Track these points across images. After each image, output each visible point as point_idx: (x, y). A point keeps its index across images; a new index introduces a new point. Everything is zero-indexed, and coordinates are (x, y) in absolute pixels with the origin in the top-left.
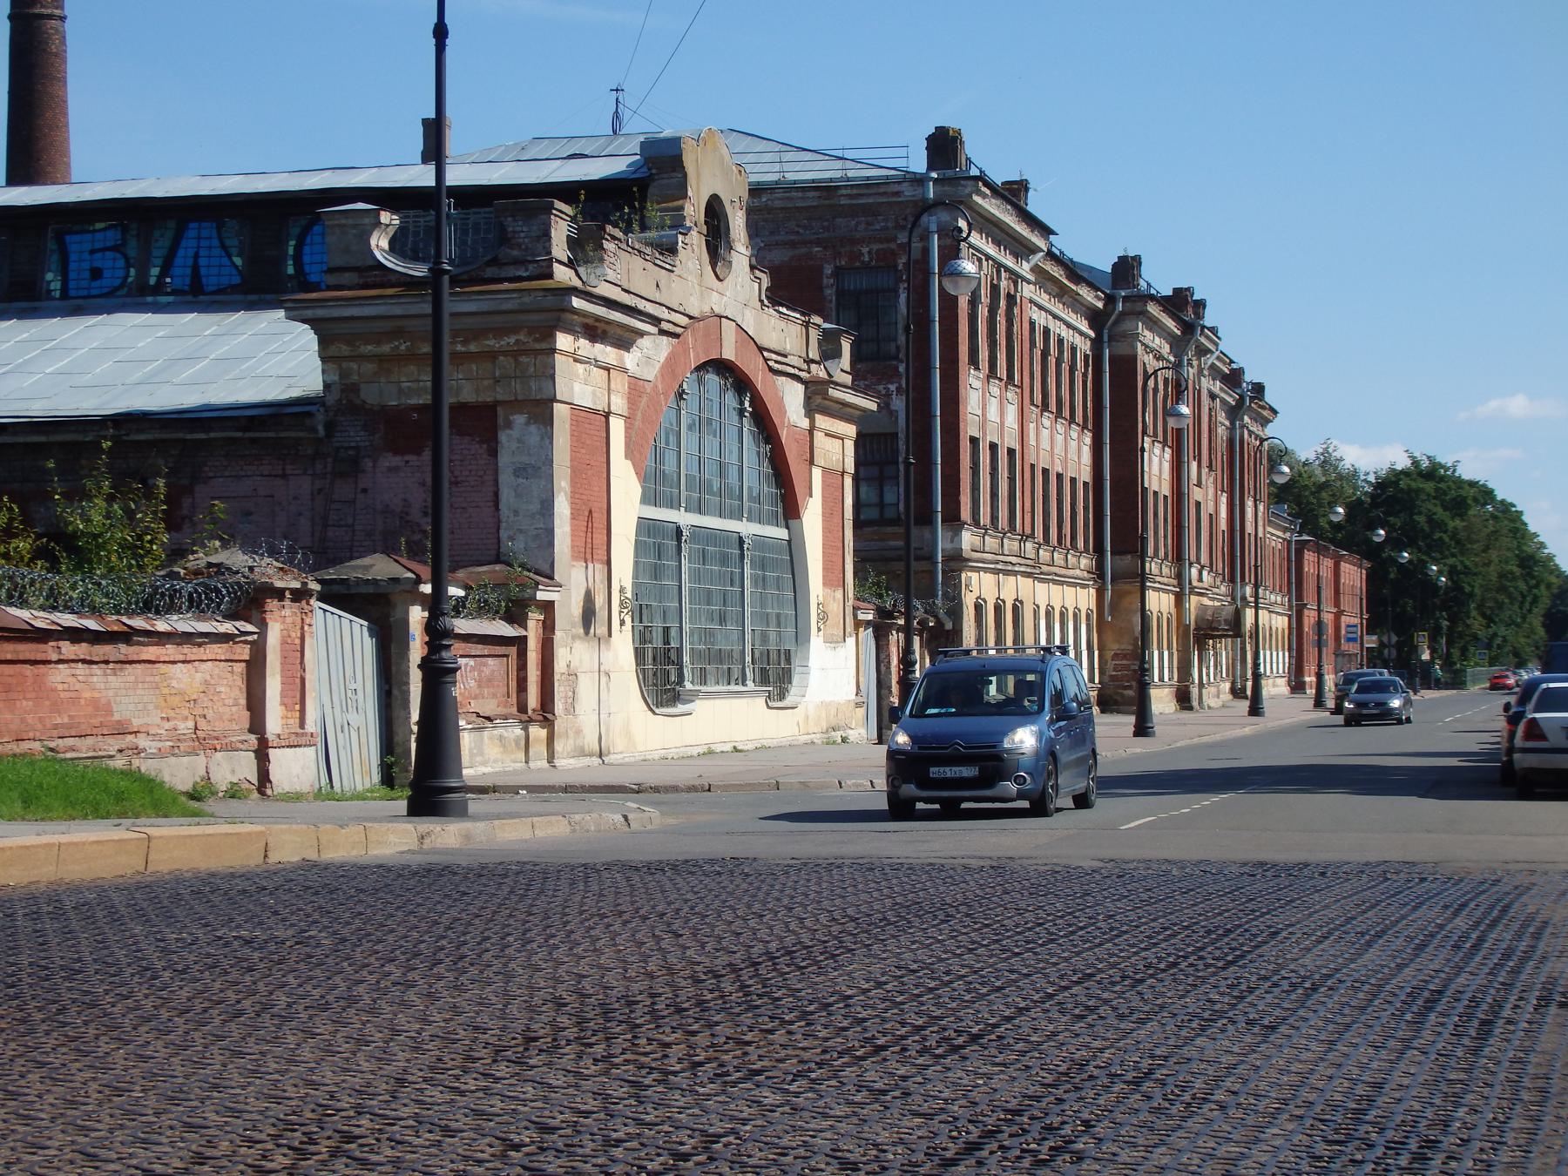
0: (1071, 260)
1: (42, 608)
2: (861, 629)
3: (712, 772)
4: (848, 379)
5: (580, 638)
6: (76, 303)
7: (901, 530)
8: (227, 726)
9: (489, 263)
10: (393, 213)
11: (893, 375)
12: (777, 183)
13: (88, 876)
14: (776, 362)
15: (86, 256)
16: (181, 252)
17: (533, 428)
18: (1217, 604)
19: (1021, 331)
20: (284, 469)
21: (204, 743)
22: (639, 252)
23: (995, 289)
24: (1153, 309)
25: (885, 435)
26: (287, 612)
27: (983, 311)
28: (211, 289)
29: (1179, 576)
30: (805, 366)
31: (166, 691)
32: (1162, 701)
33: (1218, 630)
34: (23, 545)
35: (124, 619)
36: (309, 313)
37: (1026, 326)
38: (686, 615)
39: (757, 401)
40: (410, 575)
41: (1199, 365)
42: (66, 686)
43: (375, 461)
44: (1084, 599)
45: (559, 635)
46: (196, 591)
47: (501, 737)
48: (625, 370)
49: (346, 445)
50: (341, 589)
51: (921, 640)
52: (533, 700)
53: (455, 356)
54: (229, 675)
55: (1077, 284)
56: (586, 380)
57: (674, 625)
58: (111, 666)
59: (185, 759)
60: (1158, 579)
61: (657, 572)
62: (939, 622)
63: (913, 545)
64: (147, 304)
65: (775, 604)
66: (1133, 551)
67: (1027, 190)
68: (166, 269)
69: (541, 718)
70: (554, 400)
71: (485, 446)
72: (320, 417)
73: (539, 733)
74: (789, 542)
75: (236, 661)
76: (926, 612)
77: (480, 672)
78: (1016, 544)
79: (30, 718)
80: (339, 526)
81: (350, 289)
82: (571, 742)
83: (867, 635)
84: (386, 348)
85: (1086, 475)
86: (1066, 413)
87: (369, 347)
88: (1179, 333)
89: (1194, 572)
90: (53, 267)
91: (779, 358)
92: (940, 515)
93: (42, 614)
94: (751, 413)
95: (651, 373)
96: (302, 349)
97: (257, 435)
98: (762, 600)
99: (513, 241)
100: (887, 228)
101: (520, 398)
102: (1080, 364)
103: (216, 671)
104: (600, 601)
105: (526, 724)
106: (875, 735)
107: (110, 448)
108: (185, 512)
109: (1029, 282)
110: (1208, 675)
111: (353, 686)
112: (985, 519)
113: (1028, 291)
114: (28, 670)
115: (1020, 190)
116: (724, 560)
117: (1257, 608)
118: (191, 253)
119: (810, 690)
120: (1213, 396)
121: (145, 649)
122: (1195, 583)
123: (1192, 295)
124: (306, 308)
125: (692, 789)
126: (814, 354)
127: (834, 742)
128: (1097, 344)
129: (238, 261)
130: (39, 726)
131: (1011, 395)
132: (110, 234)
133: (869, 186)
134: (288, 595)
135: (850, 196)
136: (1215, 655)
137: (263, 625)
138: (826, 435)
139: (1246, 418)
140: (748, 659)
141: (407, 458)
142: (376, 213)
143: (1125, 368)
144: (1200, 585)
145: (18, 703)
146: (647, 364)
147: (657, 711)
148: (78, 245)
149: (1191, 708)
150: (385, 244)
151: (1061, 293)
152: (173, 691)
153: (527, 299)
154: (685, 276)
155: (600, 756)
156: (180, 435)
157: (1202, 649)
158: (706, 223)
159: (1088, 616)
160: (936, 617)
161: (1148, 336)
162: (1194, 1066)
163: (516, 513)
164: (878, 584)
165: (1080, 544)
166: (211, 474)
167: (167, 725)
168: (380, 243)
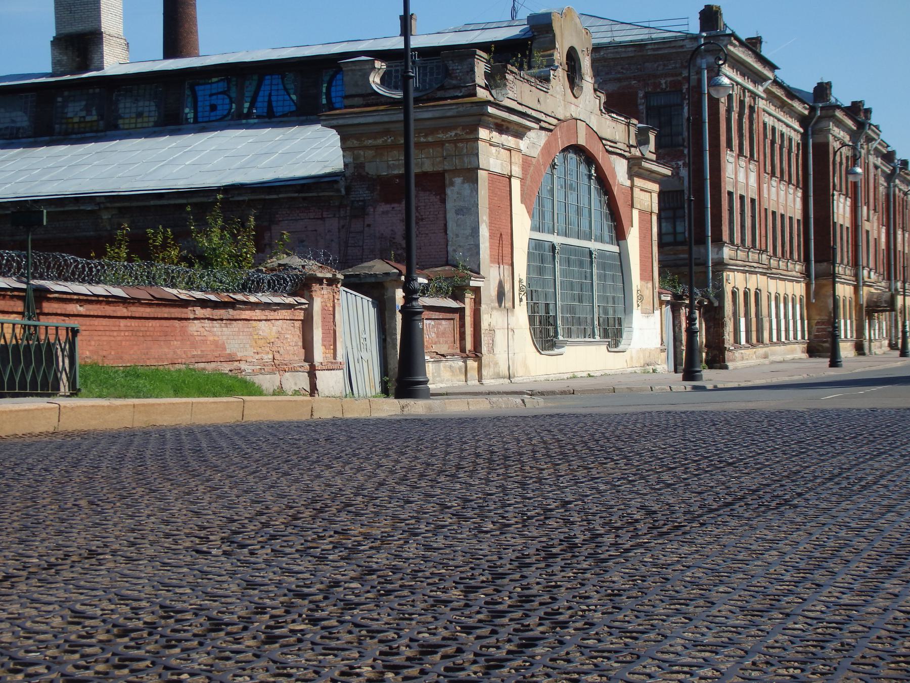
0: (788, 86)
1: (185, 289)
2: (664, 306)
3: (574, 384)
4: (654, 157)
5: (496, 309)
6: (202, 125)
7: (686, 248)
8: (292, 358)
9: (439, 89)
10: (382, 62)
11: (680, 156)
12: (609, 43)
13: (212, 422)
14: (610, 146)
15: (207, 98)
16: (261, 93)
17: (466, 186)
18: (879, 291)
19: (758, 128)
20: (322, 215)
21: (278, 367)
22: (528, 81)
23: (742, 103)
24: (839, 114)
25: (677, 191)
26: (325, 292)
27: (735, 116)
28: (278, 114)
29: (856, 275)
30: (627, 149)
31: (256, 337)
32: (846, 350)
33: (881, 307)
34: (174, 253)
35: (231, 295)
36: (335, 122)
37: (761, 125)
38: (558, 297)
39: (599, 169)
40: (395, 271)
41: (868, 148)
42: (199, 333)
43: (375, 208)
44: (799, 289)
45: (483, 307)
46: (272, 279)
47: (451, 367)
48: (520, 151)
49: (358, 199)
50: (356, 280)
51: (700, 313)
52: (469, 345)
53: (418, 145)
54: (292, 328)
55: (792, 100)
56: (497, 156)
57: (551, 302)
58: (224, 322)
59: (268, 376)
60: (843, 277)
61: (541, 271)
62: (710, 302)
63: (694, 256)
64: (242, 124)
65: (612, 290)
66: (827, 261)
67: (761, 42)
68: (253, 104)
69: (474, 355)
70: (478, 168)
71: (438, 197)
72: (342, 184)
73: (472, 364)
74: (620, 254)
75: (296, 320)
76: (702, 296)
77: (438, 328)
78: (757, 255)
79: (179, 351)
80: (355, 247)
81: (358, 107)
82: (492, 369)
83: (667, 309)
84: (379, 141)
85: (798, 215)
86: (786, 178)
87: (370, 141)
88: (855, 128)
89: (865, 272)
90: (189, 105)
91: (612, 144)
92: (710, 238)
93: (184, 291)
94: (595, 177)
95: (535, 152)
96: (332, 146)
97: (307, 195)
98: (604, 288)
99: (453, 75)
100: (676, 68)
101: (458, 168)
102: (794, 149)
103: (285, 326)
104: (507, 287)
105: (465, 359)
106: (673, 369)
107: (222, 199)
108: (266, 241)
109: (762, 99)
110: (874, 334)
111: (364, 336)
112: (737, 240)
113: (762, 104)
114: (177, 323)
115: (756, 43)
116: (581, 264)
117: (904, 295)
118: (267, 93)
119: (633, 341)
120: (876, 167)
121: (243, 312)
122: (866, 279)
123: (863, 106)
124: (334, 119)
125: (563, 393)
126: (633, 142)
127: (648, 372)
128: (804, 136)
129: (294, 97)
130: (184, 356)
131: (753, 166)
132: (221, 84)
133: (665, 43)
134: (325, 281)
135: (653, 49)
136: (879, 323)
137: (311, 299)
138: (641, 190)
139: (897, 181)
140: (596, 323)
141: (393, 206)
142: (373, 62)
143: (822, 150)
144: (869, 280)
145: (172, 343)
146: (533, 147)
147: (542, 352)
148: (203, 91)
149: (864, 354)
150: (378, 80)
151: (782, 105)
152: (260, 337)
153: (461, 109)
154: (555, 95)
155: (509, 378)
156: (263, 197)
157: (871, 319)
158: (567, 64)
159: (801, 299)
160: (708, 299)
161: (836, 131)
162: (867, 471)
163: (457, 236)
164: (673, 280)
165: (796, 257)
166: (280, 219)
167: (257, 357)
168: (375, 80)
